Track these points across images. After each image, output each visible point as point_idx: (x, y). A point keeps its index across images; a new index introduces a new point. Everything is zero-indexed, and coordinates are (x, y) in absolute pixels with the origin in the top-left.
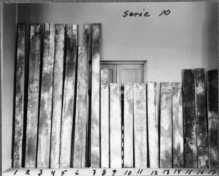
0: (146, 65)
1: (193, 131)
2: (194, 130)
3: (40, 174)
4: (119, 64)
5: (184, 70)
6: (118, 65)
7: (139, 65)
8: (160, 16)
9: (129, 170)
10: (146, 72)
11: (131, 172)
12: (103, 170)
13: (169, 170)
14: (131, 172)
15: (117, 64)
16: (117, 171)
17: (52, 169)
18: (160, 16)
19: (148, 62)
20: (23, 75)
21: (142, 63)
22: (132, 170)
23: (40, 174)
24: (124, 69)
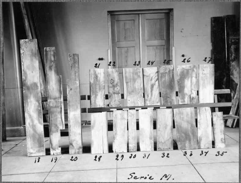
0: (172, 14)
1: (223, 84)
2: (224, 83)
3: (163, 156)
4: (141, 14)
5: (213, 17)
6: (140, 15)
7: (163, 14)
8: (149, 154)
9: (134, 154)
10: (172, 17)
11: (135, 156)
12: (116, 154)
13: (165, 152)
14: (135, 156)
15: (139, 14)
16: (124, 155)
17: (52, 155)
18: (149, 154)
19: (174, 10)
20: (30, 30)
21: (167, 11)
22: (138, 153)
23: (163, 156)
24: (147, 19)
